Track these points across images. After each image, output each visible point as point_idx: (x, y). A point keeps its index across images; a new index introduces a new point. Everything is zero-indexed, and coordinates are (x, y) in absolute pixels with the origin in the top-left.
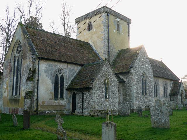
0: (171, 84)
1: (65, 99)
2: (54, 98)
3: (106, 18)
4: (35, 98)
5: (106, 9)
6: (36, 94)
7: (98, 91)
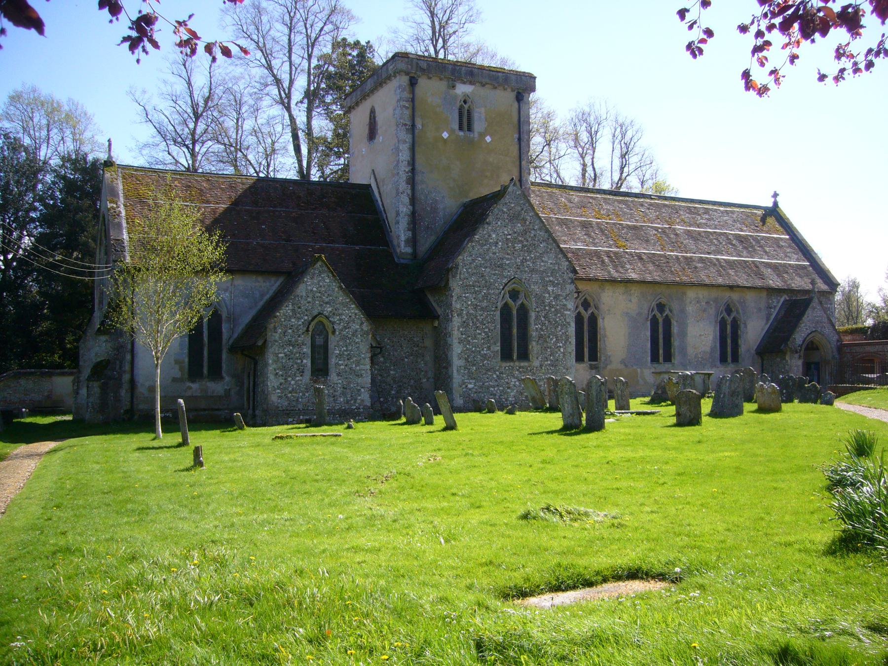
0: (769, 307)
1: (227, 379)
2: (186, 376)
3: (407, 95)
4: (126, 377)
5: (401, 65)
6: (127, 367)
7: (280, 355)
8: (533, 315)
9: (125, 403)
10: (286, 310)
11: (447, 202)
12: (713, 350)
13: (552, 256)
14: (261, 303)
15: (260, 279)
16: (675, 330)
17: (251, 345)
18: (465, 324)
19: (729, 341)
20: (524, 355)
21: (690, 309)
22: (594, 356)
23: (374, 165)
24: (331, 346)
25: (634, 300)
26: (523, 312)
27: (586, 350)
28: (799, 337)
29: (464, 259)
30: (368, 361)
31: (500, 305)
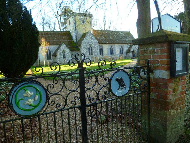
1: (52, 59)
8: (93, 49)
9: (39, 64)
10: (59, 50)
11: (81, 33)
12: (119, 52)
13: (95, 41)
14: (56, 49)
15: (56, 46)
16: (114, 50)
17: (55, 55)
18: (84, 50)
19: (122, 51)
20: (92, 54)
21: (116, 47)
22: (102, 54)
23: (70, 28)
24: (66, 54)
25: (108, 46)
26: (92, 48)
27: (101, 53)
28: (131, 50)
29: (83, 42)
30: (71, 56)
31: (88, 48)
